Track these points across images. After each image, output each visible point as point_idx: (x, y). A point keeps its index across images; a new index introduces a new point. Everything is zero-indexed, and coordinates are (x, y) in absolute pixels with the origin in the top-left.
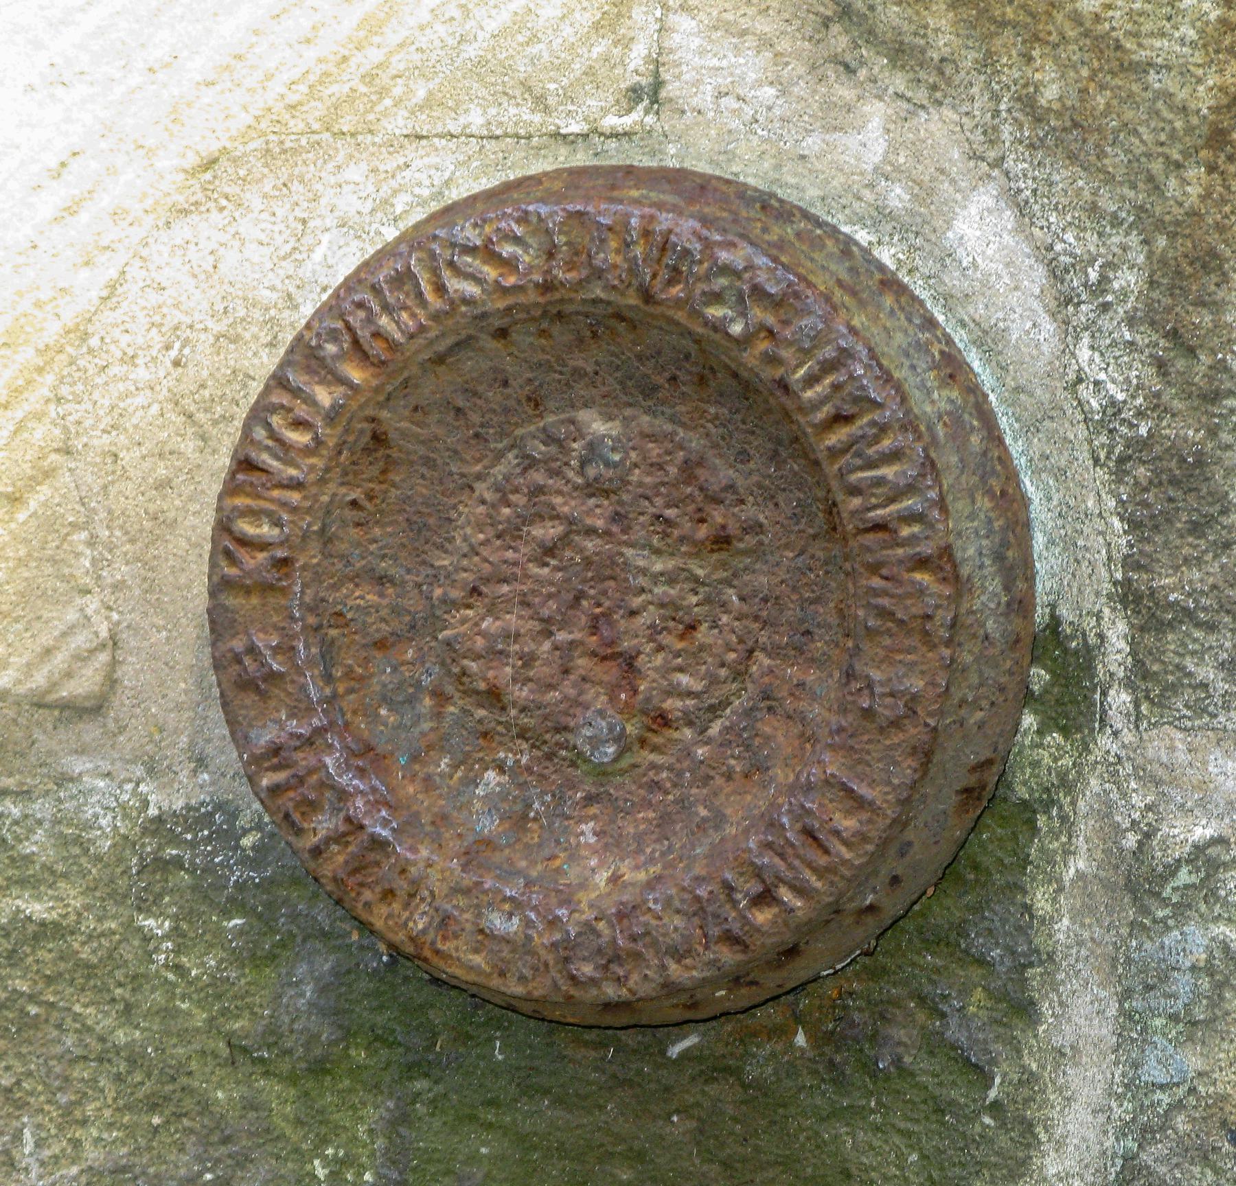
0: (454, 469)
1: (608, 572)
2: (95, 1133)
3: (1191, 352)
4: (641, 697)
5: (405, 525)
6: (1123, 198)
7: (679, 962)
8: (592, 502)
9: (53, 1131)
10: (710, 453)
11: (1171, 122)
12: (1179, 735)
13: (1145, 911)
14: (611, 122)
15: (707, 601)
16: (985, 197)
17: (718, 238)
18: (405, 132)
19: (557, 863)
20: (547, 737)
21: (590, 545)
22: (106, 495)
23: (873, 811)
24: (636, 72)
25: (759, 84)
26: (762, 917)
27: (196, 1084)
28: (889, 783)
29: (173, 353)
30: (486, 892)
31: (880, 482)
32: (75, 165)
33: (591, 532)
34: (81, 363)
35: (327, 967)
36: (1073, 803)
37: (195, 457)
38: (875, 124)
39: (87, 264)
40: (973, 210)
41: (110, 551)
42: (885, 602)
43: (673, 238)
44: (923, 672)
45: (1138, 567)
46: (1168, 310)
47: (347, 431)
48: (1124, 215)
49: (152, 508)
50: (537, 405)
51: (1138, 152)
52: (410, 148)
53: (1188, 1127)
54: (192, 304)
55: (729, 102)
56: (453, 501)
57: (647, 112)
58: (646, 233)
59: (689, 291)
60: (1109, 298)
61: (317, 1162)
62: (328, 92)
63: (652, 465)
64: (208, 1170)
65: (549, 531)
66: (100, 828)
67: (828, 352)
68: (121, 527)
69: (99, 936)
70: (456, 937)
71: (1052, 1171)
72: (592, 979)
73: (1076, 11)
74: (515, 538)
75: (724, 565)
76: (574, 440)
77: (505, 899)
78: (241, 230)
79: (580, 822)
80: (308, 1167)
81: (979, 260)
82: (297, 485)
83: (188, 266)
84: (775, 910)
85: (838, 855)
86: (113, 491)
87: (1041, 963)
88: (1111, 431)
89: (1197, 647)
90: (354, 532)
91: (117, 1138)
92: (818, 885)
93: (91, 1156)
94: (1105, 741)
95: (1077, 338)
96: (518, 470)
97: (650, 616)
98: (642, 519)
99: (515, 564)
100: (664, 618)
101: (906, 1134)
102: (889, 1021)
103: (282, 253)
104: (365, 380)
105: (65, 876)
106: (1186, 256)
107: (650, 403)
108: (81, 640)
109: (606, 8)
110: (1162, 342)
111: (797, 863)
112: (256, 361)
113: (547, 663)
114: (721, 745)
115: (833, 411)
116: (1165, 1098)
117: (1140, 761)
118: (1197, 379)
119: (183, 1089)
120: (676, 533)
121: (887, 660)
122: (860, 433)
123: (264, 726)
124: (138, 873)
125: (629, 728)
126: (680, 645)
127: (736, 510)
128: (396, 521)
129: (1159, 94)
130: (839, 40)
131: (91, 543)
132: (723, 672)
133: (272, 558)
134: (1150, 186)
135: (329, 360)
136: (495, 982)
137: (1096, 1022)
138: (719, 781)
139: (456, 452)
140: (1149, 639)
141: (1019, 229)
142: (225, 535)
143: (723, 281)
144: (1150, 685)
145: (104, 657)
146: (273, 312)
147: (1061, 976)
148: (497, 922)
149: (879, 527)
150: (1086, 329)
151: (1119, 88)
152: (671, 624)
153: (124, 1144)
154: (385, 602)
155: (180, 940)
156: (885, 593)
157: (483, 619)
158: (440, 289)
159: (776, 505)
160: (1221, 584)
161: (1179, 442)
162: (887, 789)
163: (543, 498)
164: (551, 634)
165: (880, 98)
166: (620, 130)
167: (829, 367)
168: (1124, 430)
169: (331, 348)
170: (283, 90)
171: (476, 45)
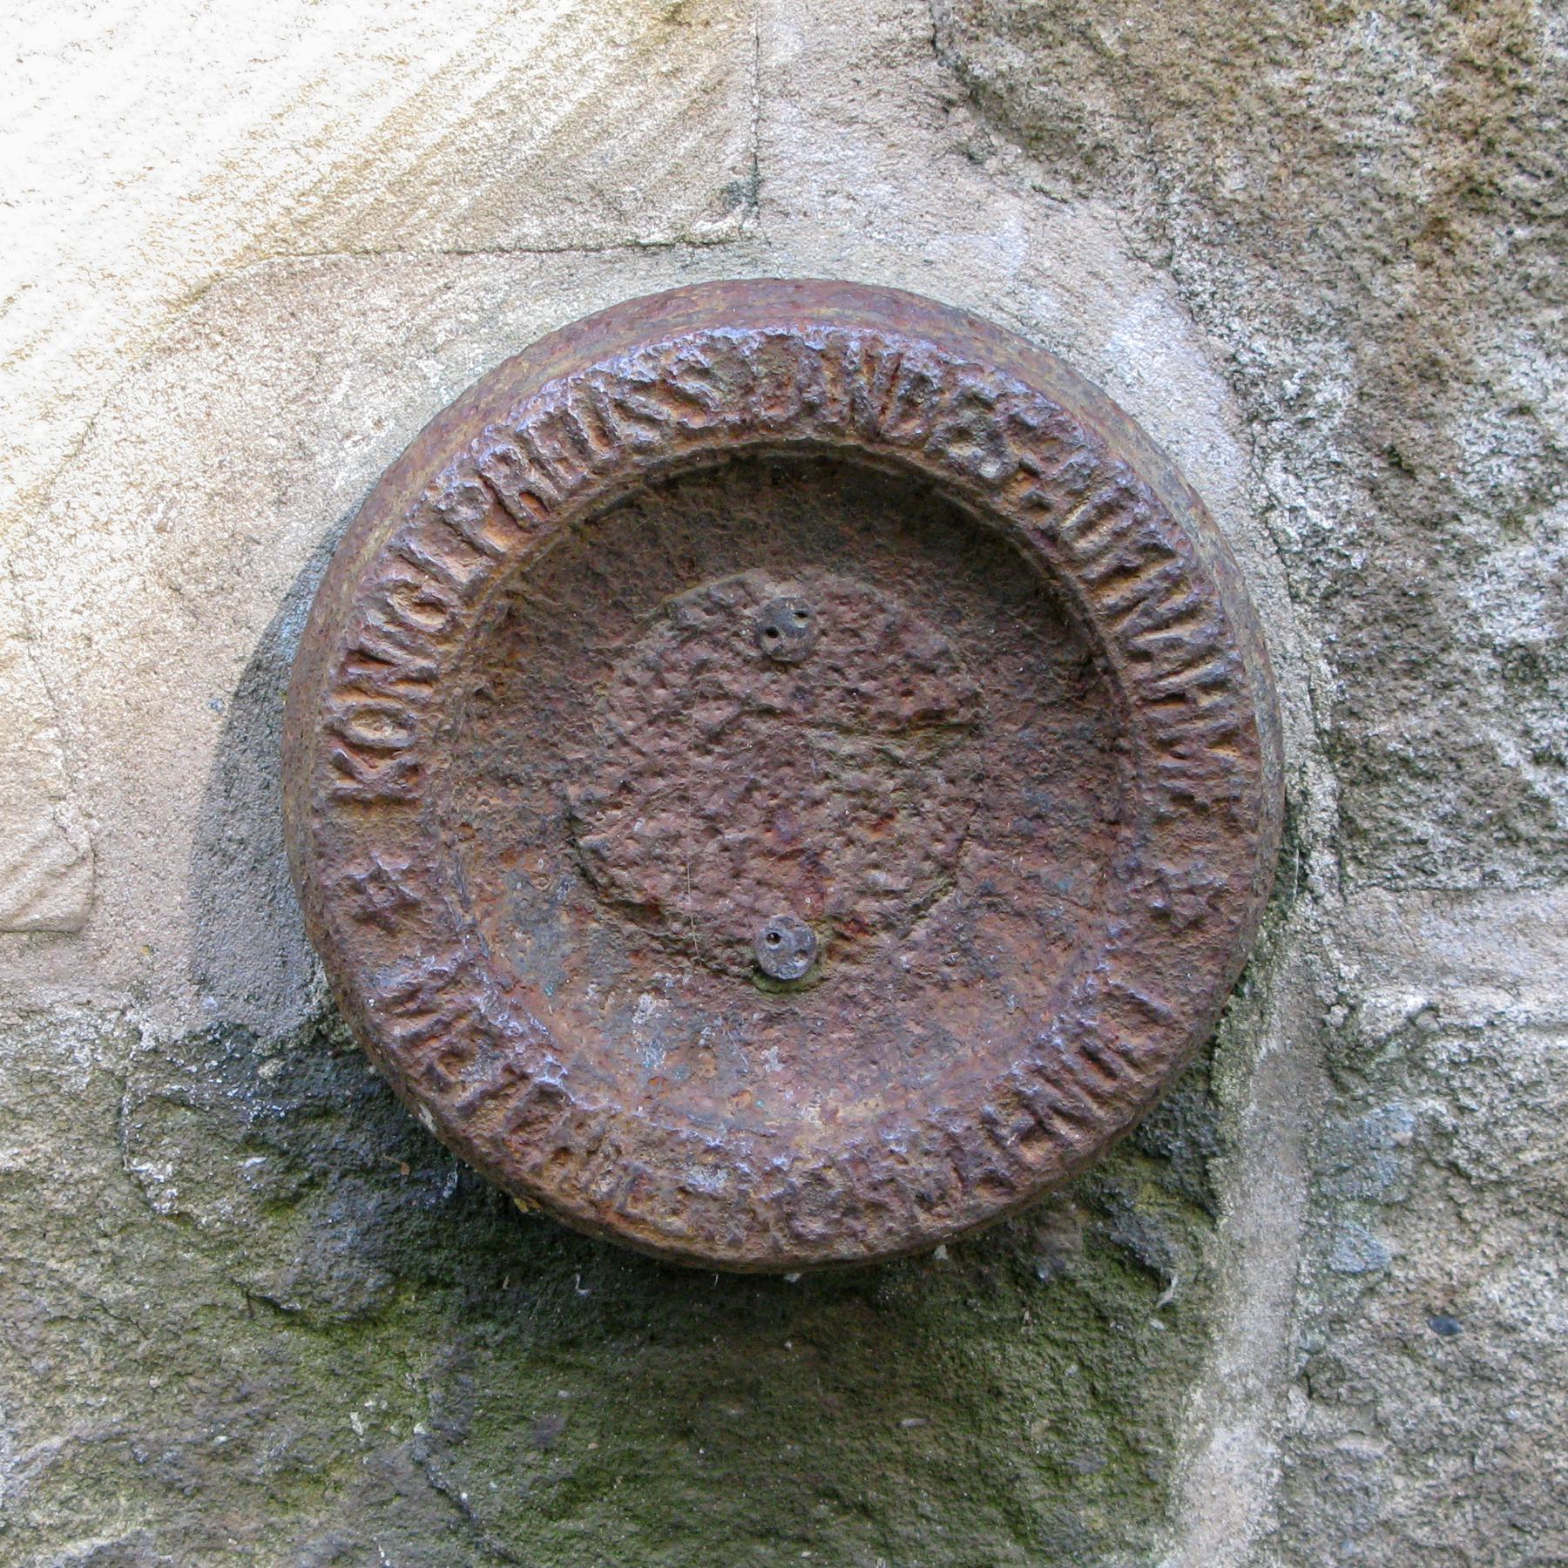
0: (590, 647)
1: (784, 757)
2: (79, 1399)
3: (1410, 473)
4: (831, 900)
5: (531, 714)
6: (1323, 301)
7: (929, 1210)
8: (766, 677)
9: (27, 1400)
10: (914, 614)
11: (1381, 212)
12: (1389, 897)
13: (1343, 1088)
14: (703, 227)
15: (908, 785)
16: (1146, 305)
17: (960, 362)
18: (445, 247)
19: (747, 1098)
20: (717, 951)
21: (763, 727)
22: (80, 685)
23: (1168, 1026)
24: (733, 169)
25: (870, 180)
26: (1033, 1154)
27: (205, 1340)
28: (1186, 992)
29: (156, 517)
30: (683, 1143)
31: (1174, 644)
32: (24, 300)
33: (769, 712)
34: (43, 533)
35: (371, 1205)
36: (1267, 978)
37: (184, 637)
38: (1012, 225)
39: (45, 417)
40: (1134, 318)
41: (86, 749)
42: (1182, 784)
43: (906, 364)
44: (1224, 863)
45: (1352, 714)
46: (1382, 426)
47: (486, 611)
48: (1323, 319)
49: (134, 697)
50: (692, 565)
51: (1340, 246)
52: (453, 264)
53: (1385, 1315)
54: (179, 459)
55: (838, 201)
56: (586, 683)
57: (745, 216)
58: (870, 359)
59: (930, 424)
60: (1312, 413)
61: (354, 1416)
62: (347, 203)
63: (843, 631)
64: (221, 1432)
65: (715, 714)
66: (76, 1062)
67: (1106, 493)
69: (76, 1184)
70: (651, 1198)
71: (1225, 1370)
72: (823, 1237)
73: (1265, 87)
74: (671, 723)
76: (745, 606)
77: (708, 1150)
78: (241, 369)
79: (760, 1048)
80: (343, 1422)
81: (1145, 375)
82: (426, 678)
83: (173, 414)
84: (1049, 1145)
85: (1127, 1079)
86: (87, 679)
87: (1224, 1153)
88: (1312, 564)
89: (1413, 799)
90: (478, 726)
91: (107, 1402)
92: (1101, 1113)
93: (78, 1424)
94: (1304, 908)
95: (1266, 460)
96: (674, 644)
97: (838, 805)
98: (828, 694)
99: (674, 753)
100: (854, 808)
101: (1066, 1345)
102: (1047, 1226)
103: (291, 394)
104: (513, 548)
105: (29, 1117)
106: (1401, 364)
107: (835, 559)
108: (56, 854)
109: (695, 95)
110: (1376, 463)
111: (1076, 1089)
112: (261, 522)
113: (715, 867)
114: (931, 950)
115: (1115, 562)
116: (1356, 1285)
117: (1344, 928)
118: (1413, 502)
119: (189, 1346)
120: (874, 709)
121: (1183, 850)
122: (1150, 587)
124: (131, 1112)
125: (818, 936)
126: (873, 838)
127: (950, 679)
128: (521, 710)
129: (1365, 182)
130: (965, 124)
131: (62, 742)
132: (928, 866)
133: (401, 766)
134: (1355, 285)
135: (466, 527)
136: (699, 1247)
137: (1280, 1211)
138: (932, 992)
139: (591, 626)
140: (1359, 794)
141: (1192, 338)
142: (334, 741)
143: (968, 415)
144: (1357, 844)
145: (85, 872)
146: (280, 465)
147: (1244, 1165)
148: (700, 1177)
149: (1177, 697)
150: (1278, 448)
151: (1317, 174)
152: (862, 814)
153: (115, 1409)
154: (510, 805)
155: (186, 1185)
156: (1183, 774)
157: (635, 820)
158: (605, 434)
159: (995, 671)
160: (1443, 729)
162: (1183, 1000)
163: (707, 675)
164: (718, 832)
165: (1014, 193)
166: (714, 238)
167: (1108, 510)
168: (1332, 562)
169: (466, 512)
170: (290, 203)
171: (532, 143)
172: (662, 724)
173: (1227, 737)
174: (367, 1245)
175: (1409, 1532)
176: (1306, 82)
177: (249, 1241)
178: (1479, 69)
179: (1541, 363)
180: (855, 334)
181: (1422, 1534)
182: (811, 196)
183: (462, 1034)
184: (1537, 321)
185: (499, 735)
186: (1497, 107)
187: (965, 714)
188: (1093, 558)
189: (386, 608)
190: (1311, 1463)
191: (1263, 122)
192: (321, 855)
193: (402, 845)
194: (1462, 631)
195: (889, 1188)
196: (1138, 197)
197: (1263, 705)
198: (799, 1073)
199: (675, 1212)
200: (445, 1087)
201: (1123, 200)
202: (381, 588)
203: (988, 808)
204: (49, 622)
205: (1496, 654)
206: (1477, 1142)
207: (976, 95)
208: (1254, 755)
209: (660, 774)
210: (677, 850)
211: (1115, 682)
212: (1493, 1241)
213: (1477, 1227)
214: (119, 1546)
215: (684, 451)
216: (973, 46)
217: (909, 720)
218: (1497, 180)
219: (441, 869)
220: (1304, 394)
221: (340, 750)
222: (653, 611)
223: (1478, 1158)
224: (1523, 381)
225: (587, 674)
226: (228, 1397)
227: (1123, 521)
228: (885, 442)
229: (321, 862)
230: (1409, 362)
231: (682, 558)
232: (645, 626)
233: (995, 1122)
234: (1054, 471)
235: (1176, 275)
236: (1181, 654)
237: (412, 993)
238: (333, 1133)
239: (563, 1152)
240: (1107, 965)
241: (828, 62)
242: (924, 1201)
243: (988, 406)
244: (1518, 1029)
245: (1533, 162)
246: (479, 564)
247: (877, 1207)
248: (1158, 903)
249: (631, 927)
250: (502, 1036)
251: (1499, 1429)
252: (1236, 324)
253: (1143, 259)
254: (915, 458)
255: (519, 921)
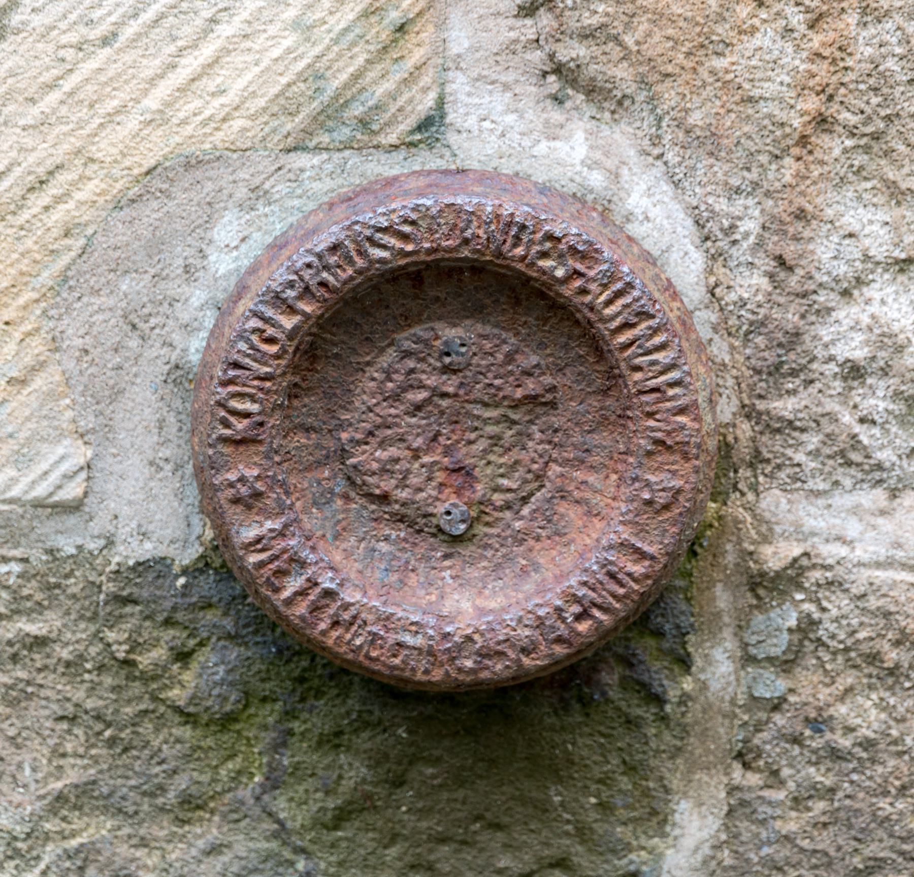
3: (791, 269)
7: (527, 656)
8: (445, 377)
15: (519, 434)
20: (419, 520)
21: (444, 403)
26: (583, 627)
28: (661, 543)
30: (399, 620)
31: (654, 363)
33: (445, 395)
42: (659, 435)
51: (753, 150)
55: (487, 124)
56: (351, 379)
67: (619, 285)
68: (92, 396)
70: (382, 648)
74: (395, 401)
75: (530, 412)
77: (412, 624)
84: (590, 622)
85: (631, 587)
92: (617, 606)
98: (478, 386)
99: (397, 416)
108: (65, 467)
111: (604, 593)
123: (250, 525)
132: (530, 476)
138: (531, 542)
143: (548, 245)
145: (83, 475)
158: (361, 253)
161: (784, 322)
164: (419, 457)
167: (619, 294)
172: (390, 401)
173: (682, 411)
174: (230, 678)
175: (798, 842)
176: (733, 64)
177: (167, 675)
178: (824, 58)
179: (861, 210)
180: (490, 203)
181: (805, 844)
182: (471, 122)
183: (285, 561)
184: (858, 188)
185: (305, 406)
186: (834, 78)
187: (549, 397)
188: (612, 318)
189: (248, 340)
190: (743, 803)
191: (711, 84)
192: (213, 468)
193: (255, 464)
194: (820, 353)
195: (508, 644)
196: (646, 123)
197: (704, 393)
198: (461, 585)
199: (395, 656)
200: (277, 590)
201: (638, 124)
202: (245, 331)
203: (561, 446)
204: (67, 343)
205: (838, 365)
206: (833, 627)
207: (558, 69)
208: (697, 419)
209: (389, 427)
210: (398, 467)
211: (624, 382)
212: (842, 683)
213: (833, 674)
214: (93, 843)
215: (402, 262)
216: (558, 44)
217: (519, 400)
218: (835, 115)
219: (275, 475)
220: (733, 227)
221: (223, 413)
222: (386, 342)
223: (833, 637)
224: (851, 220)
225: (351, 375)
226: (153, 762)
227: (628, 299)
228: (505, 258)
229: (213, 472)
230: (790, 210)
231: (401, 315)
232: (382, 350)
233: (562, 610)
234: (592, 273)
235: (666, 163)
236: (658, 368)
237: (259, 540)
238: (210, 616)
239: (336, 624)
240: (620, 528)
241: (481, 53)
242: (523, 650)
243: (559, 240)
244: (854, 566)
245: (854, 106)
246: (296, 319)
247: (501, 654)
248: (647, 496)
249: (374, 507)
250: (305, 563)
251: (846, 785)
252: (697, 190)
253: (649, 155)
254: (520, 266)
255: (315, 503)
